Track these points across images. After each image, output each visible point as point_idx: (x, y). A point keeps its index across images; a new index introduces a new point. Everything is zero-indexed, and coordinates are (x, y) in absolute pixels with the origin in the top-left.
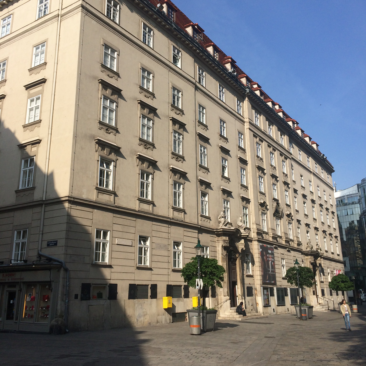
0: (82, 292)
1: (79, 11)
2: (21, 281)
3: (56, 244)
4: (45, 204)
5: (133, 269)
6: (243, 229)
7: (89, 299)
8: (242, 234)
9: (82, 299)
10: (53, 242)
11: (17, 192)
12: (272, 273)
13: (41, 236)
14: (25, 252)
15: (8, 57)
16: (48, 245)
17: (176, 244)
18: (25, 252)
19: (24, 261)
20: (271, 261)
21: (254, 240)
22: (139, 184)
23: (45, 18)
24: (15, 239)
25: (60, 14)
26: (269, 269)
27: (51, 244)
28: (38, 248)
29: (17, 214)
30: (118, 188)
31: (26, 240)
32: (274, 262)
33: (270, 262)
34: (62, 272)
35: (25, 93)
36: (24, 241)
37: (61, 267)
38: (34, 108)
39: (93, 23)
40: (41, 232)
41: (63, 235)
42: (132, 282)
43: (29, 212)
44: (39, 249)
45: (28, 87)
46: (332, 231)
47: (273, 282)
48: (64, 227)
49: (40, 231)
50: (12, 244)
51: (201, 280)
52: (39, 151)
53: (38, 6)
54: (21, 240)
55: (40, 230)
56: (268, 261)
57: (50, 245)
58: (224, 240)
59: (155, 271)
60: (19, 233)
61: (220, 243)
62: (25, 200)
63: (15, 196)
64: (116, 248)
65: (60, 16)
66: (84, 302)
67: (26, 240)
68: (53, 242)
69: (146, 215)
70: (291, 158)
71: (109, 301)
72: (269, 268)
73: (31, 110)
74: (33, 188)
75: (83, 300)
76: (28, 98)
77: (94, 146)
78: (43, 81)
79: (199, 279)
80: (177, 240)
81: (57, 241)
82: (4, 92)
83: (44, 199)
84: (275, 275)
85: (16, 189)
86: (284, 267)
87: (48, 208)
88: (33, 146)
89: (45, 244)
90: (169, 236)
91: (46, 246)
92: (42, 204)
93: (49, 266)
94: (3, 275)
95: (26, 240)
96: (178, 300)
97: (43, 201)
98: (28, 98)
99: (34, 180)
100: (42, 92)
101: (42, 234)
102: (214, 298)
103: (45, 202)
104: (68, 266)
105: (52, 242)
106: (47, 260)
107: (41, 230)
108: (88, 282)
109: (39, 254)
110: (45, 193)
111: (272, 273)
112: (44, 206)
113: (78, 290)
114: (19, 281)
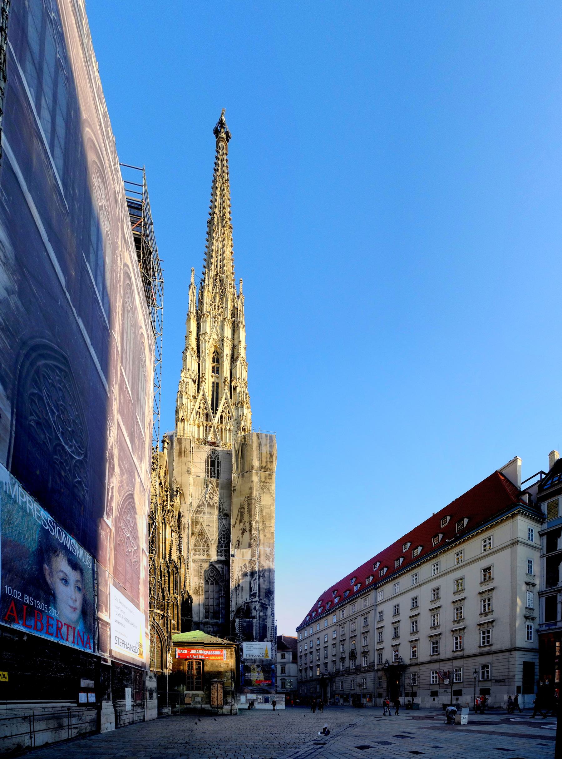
50: (430, 676)
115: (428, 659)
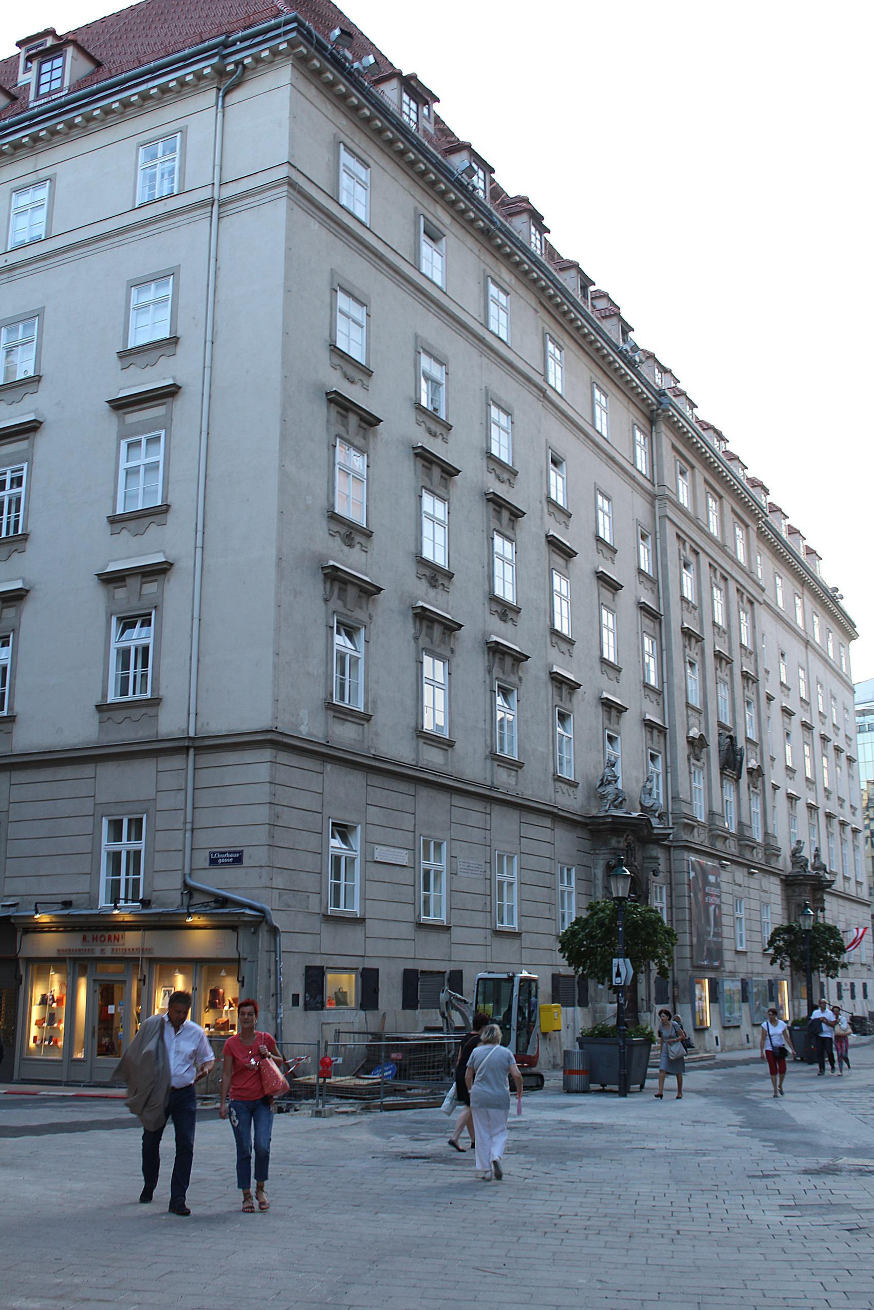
0: (307, 990)
1: (280, 195)
2: (145, 956)
3: (238, 860)
4: (195, 748)
5: (407, 930)
6: (657, 815)
7: (322, 1007)
8: (655, 831)
9: (307, 1007)
10: (230, 853)
11: (102, 708)
12: (715, 939)
13: (188, 835)
14: (141, 876)
15: (44, 307)
16: (213, 862)
17: (338, 831)
18: (141, 876)
19: (141, 901)
20: (713, 907)
21: (675, 847)
22: (133, 611)
23: (165, 204)
24: (104, 841)
25: (216, 197)
26: (708, 929)
27: (223, 860)
28: (184, 867)
29: (108, 773)
30: (375, 702)
31: (143, 844)
32: (718, 907)
33: (712, 908)
34: (263, 937)
35: (110, 422)
36: (134, 845)
37: (261, 922)
38: (142, 469)
39: (314, 227)
40: (189, 826)
41: (261, 835)
42: (410, 966)
43: (144, 770)
44: (187, 871)
45: (120, 405)
46: (845, 814)
47: (716, 964)
48: (262, 814)
49: (185, 823)
50: (95, 853)
51: (628, 960)
52: (167, 595)
53: (139, 165)
54: (125, 845)
55: (185, 819)
56: (707, 906)
57: (220, 861)
58: (614, 849)
59: (527, 940)
60: (116, 826)
61: (601, 857)
62: (128, 732)
63: (97, 722)
64: (374, 870)
65: (216, 202)
66: (313, 1014)
67: (141, 845)
68: (230, 853)
69: (439, 780)
70: (762, 601)
71: (363, 1013)
72: (708, 923)
73: (131, 472)
74: (156, 702)
75: (311, 1009)
76: (121, 437)
77: (316, 588)
78: (171, 392)
79: (621, 960)
80: (345, 818)
81: (241, 852)
82: (35, 411)
83: (192, 734)
84: (721, 943)
85: (98, 700)
86: (741, 922)
87: (207, 759)
88: (144, 580)
89: (202, 859)
90: (488, 839)
91: (207, 864)
92: (188, 748)
93: (236, 919)
94: (84, 938)
95: (141, 845)
96: (38, 969)
97: (190, 738)
98: (121, 437)
99: (155, 679)
100: (166, 423)
101: (192, 830)
102: (585, 1009)
103: (674, 844)
104: (277, 920)
105: (225, 853)
106: (215, 902)
107: (189, 819)
108: (317, 962)
109: (185, 885)
110: (192, 716)
111: (715, 939)
112: (192, 752)
113: (296, 985)
114: (140, 956)
115: (82, 730)
